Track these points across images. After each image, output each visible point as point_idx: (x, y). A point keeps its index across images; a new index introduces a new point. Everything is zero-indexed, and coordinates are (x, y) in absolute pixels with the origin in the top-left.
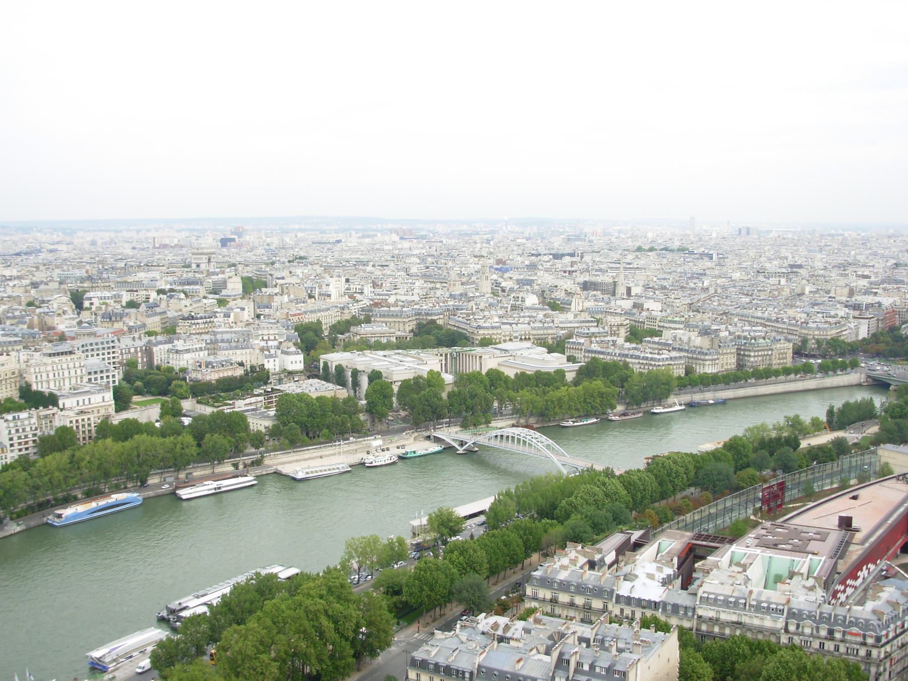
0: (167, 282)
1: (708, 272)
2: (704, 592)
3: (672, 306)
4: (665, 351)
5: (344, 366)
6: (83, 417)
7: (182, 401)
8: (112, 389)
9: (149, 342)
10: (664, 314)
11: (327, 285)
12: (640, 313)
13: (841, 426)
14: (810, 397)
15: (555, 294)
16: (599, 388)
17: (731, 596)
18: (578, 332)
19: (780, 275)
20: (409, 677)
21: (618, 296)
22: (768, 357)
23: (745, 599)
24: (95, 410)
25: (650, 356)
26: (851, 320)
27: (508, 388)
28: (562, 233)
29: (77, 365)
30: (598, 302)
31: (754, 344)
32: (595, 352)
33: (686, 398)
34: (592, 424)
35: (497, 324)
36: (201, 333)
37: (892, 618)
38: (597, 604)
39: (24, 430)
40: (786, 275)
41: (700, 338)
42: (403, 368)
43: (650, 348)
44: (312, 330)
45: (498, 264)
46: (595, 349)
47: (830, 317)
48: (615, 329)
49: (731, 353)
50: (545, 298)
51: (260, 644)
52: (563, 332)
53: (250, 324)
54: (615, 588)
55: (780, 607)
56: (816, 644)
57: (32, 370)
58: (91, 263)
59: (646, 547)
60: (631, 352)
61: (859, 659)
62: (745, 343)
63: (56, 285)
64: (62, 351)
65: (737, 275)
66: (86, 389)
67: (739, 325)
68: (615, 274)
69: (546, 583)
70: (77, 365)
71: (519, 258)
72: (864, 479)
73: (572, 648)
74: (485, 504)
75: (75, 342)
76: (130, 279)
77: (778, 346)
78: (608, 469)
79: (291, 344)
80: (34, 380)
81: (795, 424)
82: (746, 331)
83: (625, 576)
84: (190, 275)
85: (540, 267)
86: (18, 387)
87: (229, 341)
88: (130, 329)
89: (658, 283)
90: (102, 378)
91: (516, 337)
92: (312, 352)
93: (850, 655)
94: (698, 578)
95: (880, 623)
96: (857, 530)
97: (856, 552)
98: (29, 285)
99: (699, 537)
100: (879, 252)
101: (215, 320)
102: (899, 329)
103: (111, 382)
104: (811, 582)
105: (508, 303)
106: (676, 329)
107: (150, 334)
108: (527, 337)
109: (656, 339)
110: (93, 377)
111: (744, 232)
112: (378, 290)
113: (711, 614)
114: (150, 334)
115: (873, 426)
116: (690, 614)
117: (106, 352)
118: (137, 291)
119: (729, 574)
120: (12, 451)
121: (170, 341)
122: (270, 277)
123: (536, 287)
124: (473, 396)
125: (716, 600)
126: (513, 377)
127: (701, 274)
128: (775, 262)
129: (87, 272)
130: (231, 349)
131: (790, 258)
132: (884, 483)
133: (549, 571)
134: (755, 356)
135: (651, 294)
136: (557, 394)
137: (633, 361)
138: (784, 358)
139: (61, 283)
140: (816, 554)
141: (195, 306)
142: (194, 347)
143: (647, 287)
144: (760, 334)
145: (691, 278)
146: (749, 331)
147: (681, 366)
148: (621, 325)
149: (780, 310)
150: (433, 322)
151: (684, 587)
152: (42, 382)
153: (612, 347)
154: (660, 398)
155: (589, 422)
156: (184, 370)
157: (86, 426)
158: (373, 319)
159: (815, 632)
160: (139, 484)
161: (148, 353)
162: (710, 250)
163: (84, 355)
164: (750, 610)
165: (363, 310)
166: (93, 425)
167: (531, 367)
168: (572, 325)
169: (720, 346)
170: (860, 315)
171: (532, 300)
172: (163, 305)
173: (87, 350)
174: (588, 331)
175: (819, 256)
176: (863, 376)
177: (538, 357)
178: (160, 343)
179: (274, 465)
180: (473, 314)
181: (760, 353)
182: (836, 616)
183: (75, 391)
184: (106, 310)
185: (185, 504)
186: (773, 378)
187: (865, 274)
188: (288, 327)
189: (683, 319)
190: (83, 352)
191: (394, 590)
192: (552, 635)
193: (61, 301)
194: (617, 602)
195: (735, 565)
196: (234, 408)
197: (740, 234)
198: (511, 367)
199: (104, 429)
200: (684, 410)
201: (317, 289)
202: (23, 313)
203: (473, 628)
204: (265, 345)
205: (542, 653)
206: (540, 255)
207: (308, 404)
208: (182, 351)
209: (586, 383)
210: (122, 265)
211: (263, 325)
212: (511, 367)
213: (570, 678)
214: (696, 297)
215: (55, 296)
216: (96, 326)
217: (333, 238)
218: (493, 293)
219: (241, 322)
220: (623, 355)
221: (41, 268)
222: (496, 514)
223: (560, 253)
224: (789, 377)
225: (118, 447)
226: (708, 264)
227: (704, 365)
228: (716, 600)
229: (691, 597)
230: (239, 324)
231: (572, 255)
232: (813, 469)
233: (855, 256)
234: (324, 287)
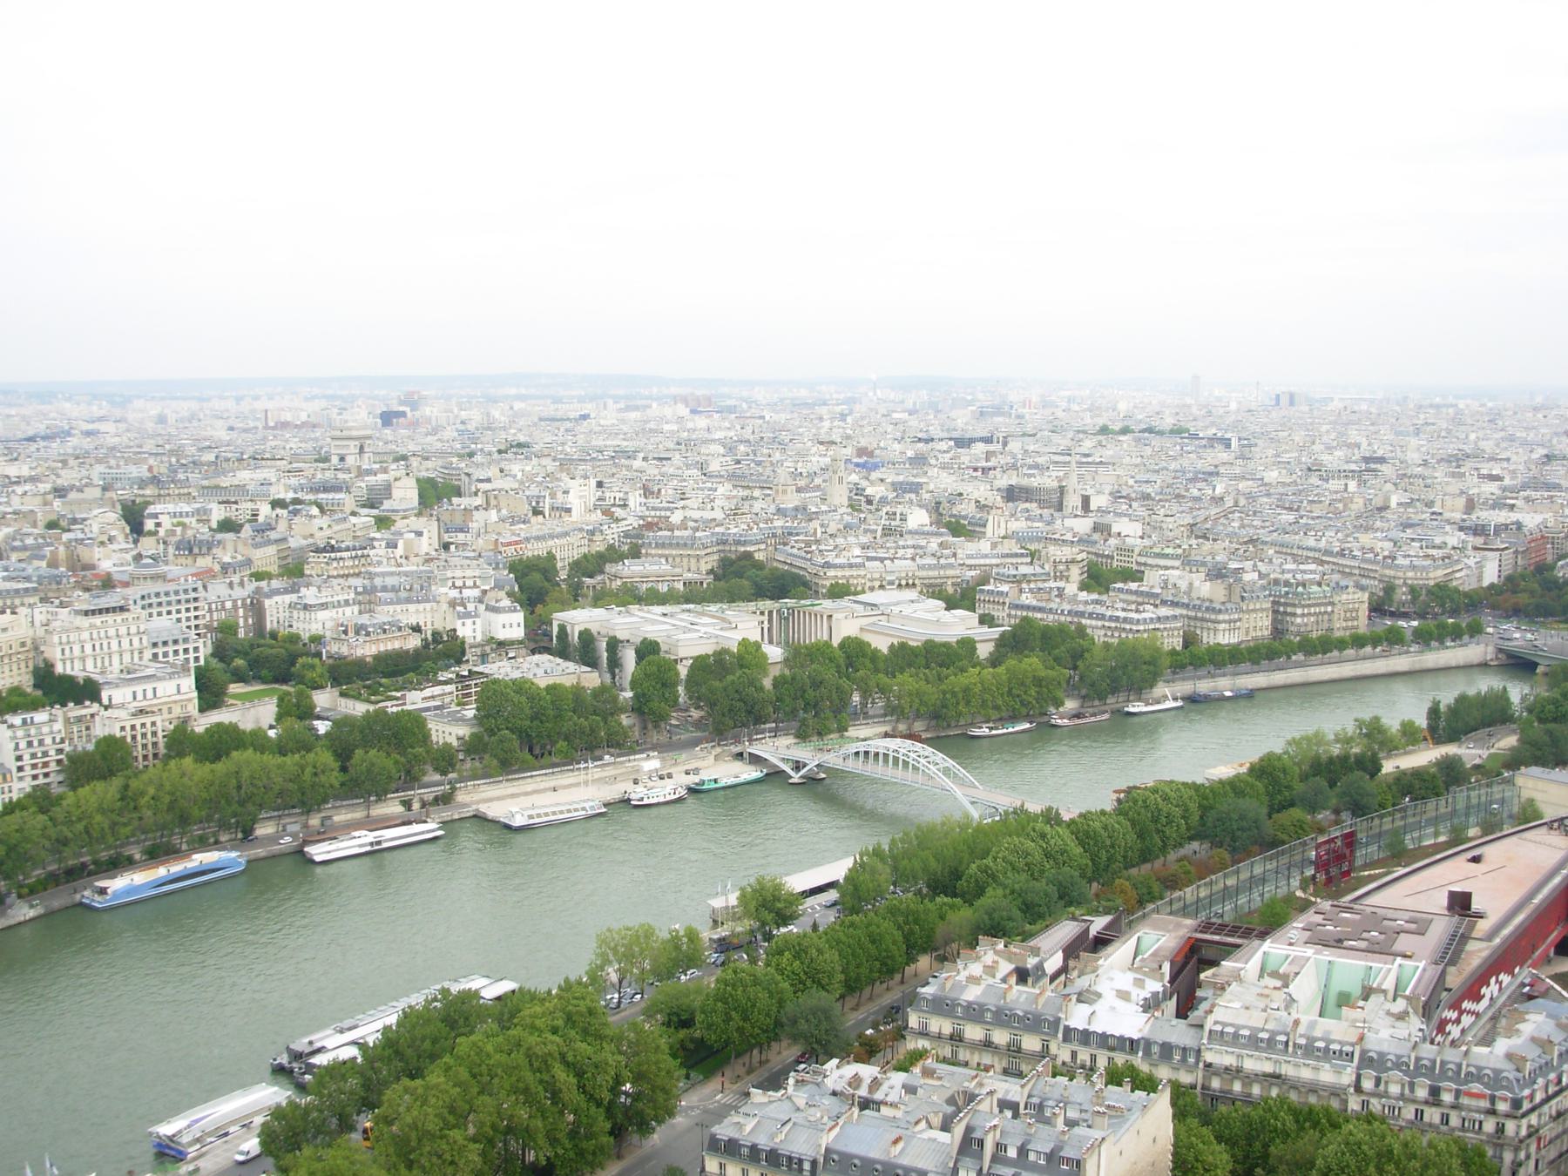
0: (288, 487)
1: (1222, 470)
2: (1216, 1023)
3: (1161, 528)
4: (1148, 607)
5: (594, 631)
6: (143, 721)
8: (193, 672)
9: (258, 590)
10: (1147, 542)
12: (1106, 540)
13: (1453, 736)
14: (1399, 686)
15: (959, 507)
16: (1035, 670)
17: (1263, 1030)
18: (998, 574)
19: (1347, 475)
21: (1067, 510)
22: (1326, 617)
23: (1287, 1034)
24: (165, 708)
25: (1122, 614)
26: (1470, 552)
27: (877, 670)
28: (970, 403)
30: (1033, 521)
31: (1302, 594)
32: (1028, 608)
33: (1185, 687)
34: (1023, 731)
35: (859, 560)
37: (1541, 1068)
38: (1031, 1043)
39: (41, 743)
40: (1358, 475)
41: (1208, 583)
42: (695, 635)
43: (1122, 600)
44: (539, 570)
45: (859, 456)
47: (1434, 547)
48: (1061, 567)
49: (1262, 610)
50: (941, 515)
51: (450, 1113)
52: (973, 573)
53: (432, 559)
54: (1062, 1016)
55: (1347, 1049)
56: (1409, 1113)
59: (1115, 945)
60: (1090, 608)
61: (1484, 1138)
62: (1287, 593)
63: (97, 492)
64: (107, 606)
65: (1272, 476)
66: (149, 672)
67: (1277, 561)
68: (1061, 474)
69: (942, 1006)
70: (133, 630)
72: (1492, 828)
73: (987, 1118)
74: (837, 870)
75: (129, 591)
76: (225, 482)
77: (1344, 597)
78: (1049, 809)
79: (502, 594)
81: (1373, 731)
82: (1289, 571)
83: (1080, 994)
84: (329, 475)
85: (933, 462)
86: (31, 668)
87: (395, 590)
88: (225, 568)
89: (1136, 488)
90: (176, 652)
91: (890, 583)
92: (539, 608)
93: (1468, 1131)
94: (1206, 999)
95: (1520, 1075)
96: (1480, 916)
97: (1478, 952)
98: (49, 493)
99: (1207, 927)
100: (1518, 435)
101: (372, 552)
102: (1552, 567)
103: (192, 660)
104: (1401, 1005)
105: (877, 523)
106: (1167, 568)
107: (258, 576)
108: (911, 582)
109: (1133, 586)
110: (160, 650)
111: (1284, 400)
112: (652, 502)
113: (1228, 1060)
114: (258, 576)
115: (1508, 735)
116: (1191, 1060)
118: (236, 503)
119: (1260, 991)
120: (21, 779)
122: (467, 479)
123: (926, 496)
124: (817, 684)
125: (1236, 1035)
126: (885, 651)
127: (1211, 474)
128: (1338, 453)
129: (150, 469)
130: (399, 602)
131: (1364, 446)
132: (1527, 835)
133: (948, 985)
134: (1303, 615)
135: (1125, 507)
136: (962, 680)
137: (1094, 623)
138: (1354, 619)
139: (105, 489)
140: (1410, 957)
141: (336, 528)
142: (336, 599)
143: (1116, 496)
144: (1312, 576)
145: (1194, 480)
146: (1294, 572)
147: (1176, 633)
148: (1073, 561)
149: (1347, 536)
150: (748, 556)
151: (1182, 1013)
153: (1058, 600)
154: (1139, 688)
155: (1017, 729)
156: (317, 639)
157: (149, 736)
158: (643, 551)
159: (1407, 1091)
160: (240, 835)
162: (1226, 431)
164: (1295, 1054)
165: (627, 535)
166: (160, 734)
167: (917, 634)
168: (988, 561)
169: (1243, 598)
170: (1485, 544)
171: (918, 518)
172: (282, 527)
173: (150, 605)
174: (1015, 572)
175: (1414, 442)
176: (1491, 649)
177: (929, 616)
178: (277, 592)
179: (473, 803)
180: (817, 542)
181: (1312, 610)
182: (1443, 1063)
183: (130, 676)
184: (182, 535)
185: (319, 870)
186: (1335, 653)
187: (1494, 473)
188: (497, 564)
189: (1180, 551)
191: (680, 1020)
192: (953, 1096)
193: (106, 520)
194: (1066, 1039)
195: (1269, 975)
196: (404, 704)
197: (1278, 403)
198: (883, 634)
199: (180, 741)
200: (1182, 707)
202: (40, 541)
203: (817, 1084)
204: (458, 596)
205: (936, 1128)
206: (932, 440)
207: (531, 698)
208: (315, 606)
209: (1011, 662)
211: (454, 561)
212: (883, 634)
213: (985, 1170)
214: (1202, 514)
215: (96, 512)
216: (167, 563)
217: (575, 411)
218: (851, 506)
219: (417, 555)
220: (1076, 612)
221: (72, 462)
222: (856, 888)
223: (968, 436)
224: (1362, 652)
225: (204, 771)
226: (1223, 456)
227: (1216, 630)
228: (1236, 1035)
229: (1193, 1031)
230: (412, 559)
231: (987, 440)
232: (1404, 810)
233: (1476, 443)
234: (559, 495)
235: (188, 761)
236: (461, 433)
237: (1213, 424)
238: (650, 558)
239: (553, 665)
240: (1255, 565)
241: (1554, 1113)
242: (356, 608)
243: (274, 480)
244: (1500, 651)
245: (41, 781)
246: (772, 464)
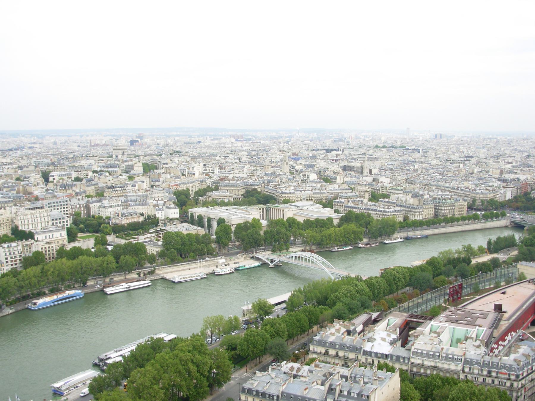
0: (98, 166)
1: (417, 160)
2: (415, 349)
3: (396, 180)
4: (392, 207)
5: (203, 215)
6: (49, 246)
7: (107, 236)
8: (66, 229)
9: (88, 201)
10: (391, 185)
11: (193, 168)
12: (377, 184)
13: (496, 251)
14: (477, 234)
15: (327, 173)
16: (353, 229)
17: (431, 351)
18: (340, 196)
19: (459, 162)
21: (364, 174)
22: (452, 210)
23: (439, 353)
24: (56, 242)
25: (383, 209)
26: (502, 188)
28: (331, 137)
30: (353, 178)
31: (444, 203)
32: (351, 207)
33: (404, 234)
34: (349, 249)
35: (293, 191)
37: (526, 364)
38: (352, 356)
39: (14, 253)
40: (463, 162)
41: (412, 199)
42: (237, 217)
43: (383, 205)
45: (293, 155)
46: (350, 205)
47: (489, 187)
48: (362, 193)
49: (431, 208)
50: (321, 176)
51: (153, 379)
52: (332, 195)
53: (147, 191)
54: (362, 346)
55: (460, 358)
56: (481, 379)
59: (381, 322)
60: (372, 207)
61: (506, 388)
62: (439, 202)
63: (33, 168)
64: (36, 207)
65: (434, 162)
66: (51, 229)
67: (436, 191)
68: (362, 161)
69: (321, 343)
70: (46, 215)
72: (509, 282)
73: (337, 381)
74: (286, 297)
75: (44, 202)
76: (77, 164)
77: (459, 203)
78: (358, 276)
79: (171, 203)
81: (469, 249)
82: (440, 195)
83: (368, 339)
84: (112, 162)
85: (318, 157)
86: (11, 228)
87: (135, 201)
88: (77, 194)
89: (388, 166)
90: (60, 222)
91: (304, 199)
92: (184, 207)
93: (501, 386)
94: (411, 341)
95: (519, 367)
96: (505, 312)
97: (504, 325)
98: (17, 168)
99: (412, 316)
100: (518, 148)
101: (127, 188)
102: (530, 193)
103: (65, 225)
104: (478, 343)
105: (299, 178)
106: (398, 194)
107: (88, 196)
108: (311, 198)
109: (387, 200)
110: (55, 222)
111: (438, 137)
112: (223, 171)
113: (419, 362)
114: (88, 196)
115: (514, 251)
116: (407, 362)
118: (80, 171)
119: (430, 338)
120: (7, 266)
122: (159, 163)
123: (316, 169)
124: (279, 233)
125: (422, 353)
126: (302, 222)
127: (413, 162)
128: (456, 155)
129: (51, 160)
130: (136, 205)
131: (465, 152)
132: (521, 285)
133: (324, 336)
134: (445, 210)
135: (384, 173)
136: (328, 232)
137: (373, 212)
138: (462, 211)
139: (36, 167)
140: (481, 326)
141: (115, 180)
142: (115, 204)
143: (381, 169)
144: (448, 197)
145: (407, 164)
146: (441, 195)
147: (401, 216)
148: (366, 191)
149: (460, 183)
150: (255, 190)
151: (403, 346)
153: (361, 205)
154: (389, 235)
155: (347, 248)
156: (108, 218)
157: (51, 251)
158: (220, 188)
159: (480, 372)
160: (82, 285)
162: (418, 147)
164: (442, 359)
165: (214, 182)
166: (55, 250)
167: (313, 216)
168: (337, 191)
169: (424, 204)
170: (507, 185)
171: (313, 177)
172: (96, 180)
173: (51, 206)
174: (346, 195)
175: (482, 151)
176: (509, 221)
177: (317, 210)
178: (94, 202)
179: (161, 274)
180: (279, 185)
181: (448, 208)
182: (492, 362)
183: (44, 230)
184: (62, 183)
185: (109, 297)
186: (456, 223)
187: (510, 161)
188: (170, 192)
189: (402, 188)
191: (232, 348)
192: (325, 374)
193: (36, 177)
194: (364, 354)
195: (433, 332)
196: (138, 240)
197: (436, 138)
198: (301, 216)
199: (61, 253)
200: (403, 241)
202: (14, 184)
203: (279, 370)
204: (156, 203)
205: (319, 385)
206: (318, 150)
207: (181, 238)
208: (107, 207)
209: (345, 226)
211: (155, 191)
212: (301, 216)
213: (336, 399)
214: (410, 175)
215: (33, 175)
216: (57, 192)
218: (290, 172)
219: (142, 189)
220: (367, 209)
221: (24, 158)
222: (292, 303)
223: (330, 149)
224: (465, 222)
225: (69, 263)
226: (417, 155)
227: (415, 215)
228: (422, 353)
229: (407, 352)
230: (141, 191)
231: (337, 150)
232: (479, 276)
233: (504, 151)
234: (191, 169)
235: (64, 260)
236: (157, 148)
237: (414, 145)
239: (189, 227)
240: (428, 193)
241: (530, 379)
242: (121, 207)
243: (93, 164)
245: (14, 266)
246: (263, 158)
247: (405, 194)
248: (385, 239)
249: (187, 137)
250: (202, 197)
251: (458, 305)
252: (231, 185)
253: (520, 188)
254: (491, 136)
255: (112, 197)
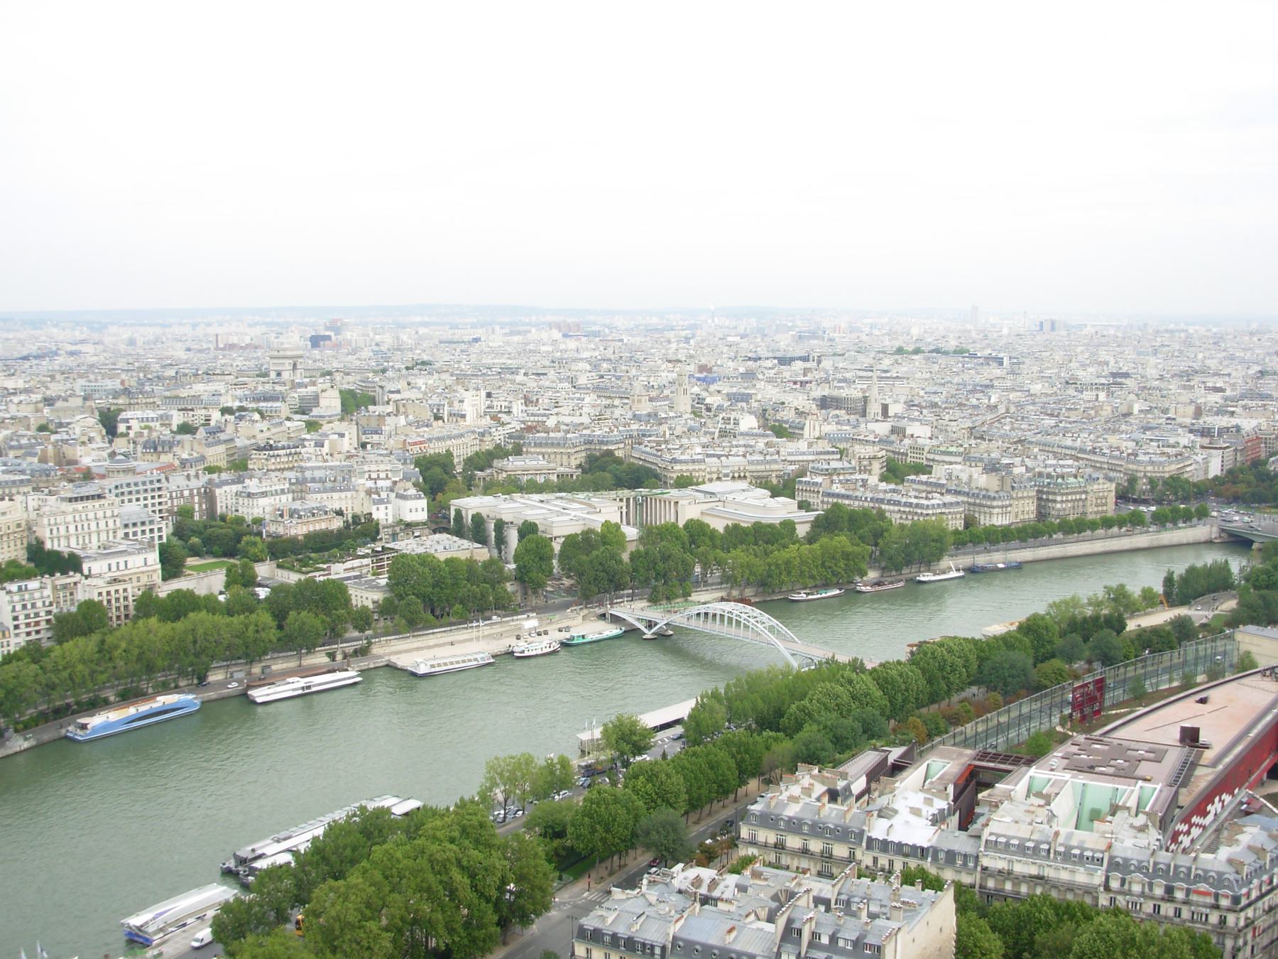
0: (235, 398)
1: (996, 383)
2: (991, 834)
3: (946, 431)
4: (935, 495)
5: (484, 515)
6: (117, 588)
7: (256, 565)
8: (157, 548)
9: (210, 481)
10: (934, 442)
11: (460, 401)
12: (901, 441)
13: (1184, 601)
14: (1140, 560)
15: (782, 414)
16: (843, 547)
17: (1029, 840)
18: (813, 468)
19: (1098, 387)
20: (576, 953)
21: (870, 416)
22: (1081, 503)
23: (1049, 844)
24: (134, 578)
25: (914, 501)
26: (1198, 450)
27: (715, 547)
29: (109, 513)
30: (842, 425)
32: (838, 496)
33: (966, 560)
34: (834, 596)
35: (700, 457)
36: (283, 470)
37: (1256, 871)
38: (840, 851)
39: (33, 606)
41: (985, 476)
42: (567, 518)
43: (914, 490)
45: (700, 372)
46: (837, 491)
47: (1169, 446)
48: (865, 463)
49: (1029, 497)
50: (767, 420)
51: (366, 907)
52: (793, 467)
53: (352, 456)
54: (866, 828)
55: (1098, 855)
56: (1148, 907)
57: (46, 521)
58: (128, 371)
59: (909, 770)
60: (888, 496)
61: (1210, 928)
62: (1049, 484)
63: (79, 402)
64: (87, 494)
65: (1037, 388)
66: (121, 548)
67: (1040, 458)
68: (865, 386)
70: (109, 513)
71: (731, 364)
72: (1216, 675)
73: (805, 912)
74: (683, 710)
75: (105, 482)
76: (183, 393)
77: (1096, 487)
78: (855, 660)
79: (409, 484)
80: (48, 534)
81: (1119, 596)
82: (1051, 466)
83: (880, 811)
84: (268, 387)
85: (760, 376)
86: (25, 545)
87: (322, 481)
89: (926, 398)
90: (143, 532)
91: (726, 475)
92: (440, 496)
93: (1196, 922)
94: (983, 815)
95: (1239, 877)
96: (1206, 747)
97: (1204, 777)
98: (40, 402)
99: (984, 756)
100: (1237, 354)
101: (303, 451)
102: (1265, 463)
103: (156, 539)
104: (1142, 819)
105: (715, 426)
107: (211, 470)
108: (742, 474)
109: (924, 478)
110: (130, 530)
111: (1047, 327)
112: (532, 409)
113: (1001, 865)
114: (211, 470)
115: (1229, 599)
116: (971, 865)
117: (149, 496)
118: (192, 410)
119: (1027, 808)
120: (17, 635)
121: (240, 481)
122: (380, 391)
123: (755, 405)
124: (666, 558)
125: (1007, 844)
126: (721, 531)
127: (987, 386)
128: (1090, 370)
129: (123, 382)
130: (325, 491)
131: (1112, 363)
132: (1245, 681)
133: (773, 804)
134: (1062, 502)
135: (917, 413)
136: (784, 555)
137: (892, 508)
138: (1103, 505)
139: (85, 399)
140: (1149, 780)
141: (274, 430)
142: (274, 488)
143: (910, 405)
144: (1069, 470)
145: (973, 391)
146: (1055, 466)
147: (958, 516)
148: (875, 458)
149: (1098, 437)
150: (610, 453)
151: (963, 826)
152: (59, 539)
153: (862, 489)
154: (929, 561)
155: (829, 594)
156: (258, 521)
157: (122, 600)
158: (524, 450)
159: (1147, 890)
160: (196, 681)
161: (209, 496)
163: (118, 500)
164: (1055, 860)
165: (511, 436)
166: (131, 599)
167: (747, 517)
168: (805, 458)
169: (1013, 488)
170: (1210, 443)
171: (748, 422)
172: (230, 429)
173: (123, 494)
174: (827, 467)
175: (1153, 360)
176: (1215, 529)
177: (757, 502)
178: (226, 483)
179: (385, 655)
180: (666, 442)
181: (1070, 498)
182: (1176, 867)
183: (106, 551)
184: (149, 436)
185: (260, 709)
186: (1088, 533)
187: (1218, 385)
188: (405, 460)
189: (961, 449)
190: (117, 496)
191: (554, 832)
192: (777, 894)
193: (86, 424)
194: (869, 847)
195: (1034, 795)
196: (330, 574)
197: (1041, 329)
198: (719, 517)
199: (147, 604)
200: (963, 577)
201: (446, 408)
202: (33, 441)
203: (666, 884)
204: (373, 486)
205: (763, 920)
206: (760, 359)
207: (433, 569)
208: (256, 494)
209: (824, 540)
210: (172, 373)
211: (370, 457)
212: (719, 517)
213: (803, 954)
214: (980, 419)
215: (78, 417)
216: (136, 459)
218: (693, 413)
219: (340, 453)
220: (877, 499)
221: (58, 377)
222: (698, 724)
223: (789, 356)
224: (1110, 531)
225: (166, 629)
226: (997, 372)
227: (991, 514)
228: (1007, 844)
229: (972, 841)
230: (336, 456)
231: (805, 359)
232: (1144, 660)
233: (1203, 361)
234: (456, 404)
235: (153, 621)
236: (376, 353)
237: (988, 346)
238: (530, 455)
240: (1023, 461)
241: (1266, 907)
242: (290, 496)
244: (1223, 530)
246: (629, 378)
247: (968, 463)
248: (920, 572)
249: (447, 327)
250: (482, 470)
251: (1094, 731)
252: (552, 444)
253: (1241, 450)
254: (1172, 326)
255: (268, 470)
